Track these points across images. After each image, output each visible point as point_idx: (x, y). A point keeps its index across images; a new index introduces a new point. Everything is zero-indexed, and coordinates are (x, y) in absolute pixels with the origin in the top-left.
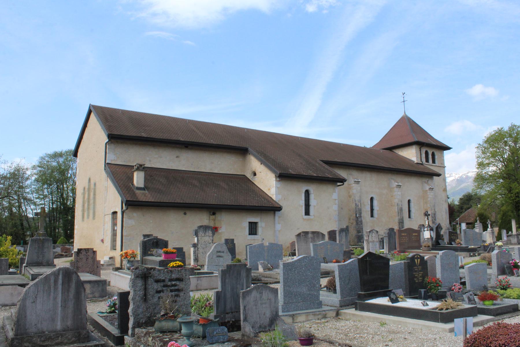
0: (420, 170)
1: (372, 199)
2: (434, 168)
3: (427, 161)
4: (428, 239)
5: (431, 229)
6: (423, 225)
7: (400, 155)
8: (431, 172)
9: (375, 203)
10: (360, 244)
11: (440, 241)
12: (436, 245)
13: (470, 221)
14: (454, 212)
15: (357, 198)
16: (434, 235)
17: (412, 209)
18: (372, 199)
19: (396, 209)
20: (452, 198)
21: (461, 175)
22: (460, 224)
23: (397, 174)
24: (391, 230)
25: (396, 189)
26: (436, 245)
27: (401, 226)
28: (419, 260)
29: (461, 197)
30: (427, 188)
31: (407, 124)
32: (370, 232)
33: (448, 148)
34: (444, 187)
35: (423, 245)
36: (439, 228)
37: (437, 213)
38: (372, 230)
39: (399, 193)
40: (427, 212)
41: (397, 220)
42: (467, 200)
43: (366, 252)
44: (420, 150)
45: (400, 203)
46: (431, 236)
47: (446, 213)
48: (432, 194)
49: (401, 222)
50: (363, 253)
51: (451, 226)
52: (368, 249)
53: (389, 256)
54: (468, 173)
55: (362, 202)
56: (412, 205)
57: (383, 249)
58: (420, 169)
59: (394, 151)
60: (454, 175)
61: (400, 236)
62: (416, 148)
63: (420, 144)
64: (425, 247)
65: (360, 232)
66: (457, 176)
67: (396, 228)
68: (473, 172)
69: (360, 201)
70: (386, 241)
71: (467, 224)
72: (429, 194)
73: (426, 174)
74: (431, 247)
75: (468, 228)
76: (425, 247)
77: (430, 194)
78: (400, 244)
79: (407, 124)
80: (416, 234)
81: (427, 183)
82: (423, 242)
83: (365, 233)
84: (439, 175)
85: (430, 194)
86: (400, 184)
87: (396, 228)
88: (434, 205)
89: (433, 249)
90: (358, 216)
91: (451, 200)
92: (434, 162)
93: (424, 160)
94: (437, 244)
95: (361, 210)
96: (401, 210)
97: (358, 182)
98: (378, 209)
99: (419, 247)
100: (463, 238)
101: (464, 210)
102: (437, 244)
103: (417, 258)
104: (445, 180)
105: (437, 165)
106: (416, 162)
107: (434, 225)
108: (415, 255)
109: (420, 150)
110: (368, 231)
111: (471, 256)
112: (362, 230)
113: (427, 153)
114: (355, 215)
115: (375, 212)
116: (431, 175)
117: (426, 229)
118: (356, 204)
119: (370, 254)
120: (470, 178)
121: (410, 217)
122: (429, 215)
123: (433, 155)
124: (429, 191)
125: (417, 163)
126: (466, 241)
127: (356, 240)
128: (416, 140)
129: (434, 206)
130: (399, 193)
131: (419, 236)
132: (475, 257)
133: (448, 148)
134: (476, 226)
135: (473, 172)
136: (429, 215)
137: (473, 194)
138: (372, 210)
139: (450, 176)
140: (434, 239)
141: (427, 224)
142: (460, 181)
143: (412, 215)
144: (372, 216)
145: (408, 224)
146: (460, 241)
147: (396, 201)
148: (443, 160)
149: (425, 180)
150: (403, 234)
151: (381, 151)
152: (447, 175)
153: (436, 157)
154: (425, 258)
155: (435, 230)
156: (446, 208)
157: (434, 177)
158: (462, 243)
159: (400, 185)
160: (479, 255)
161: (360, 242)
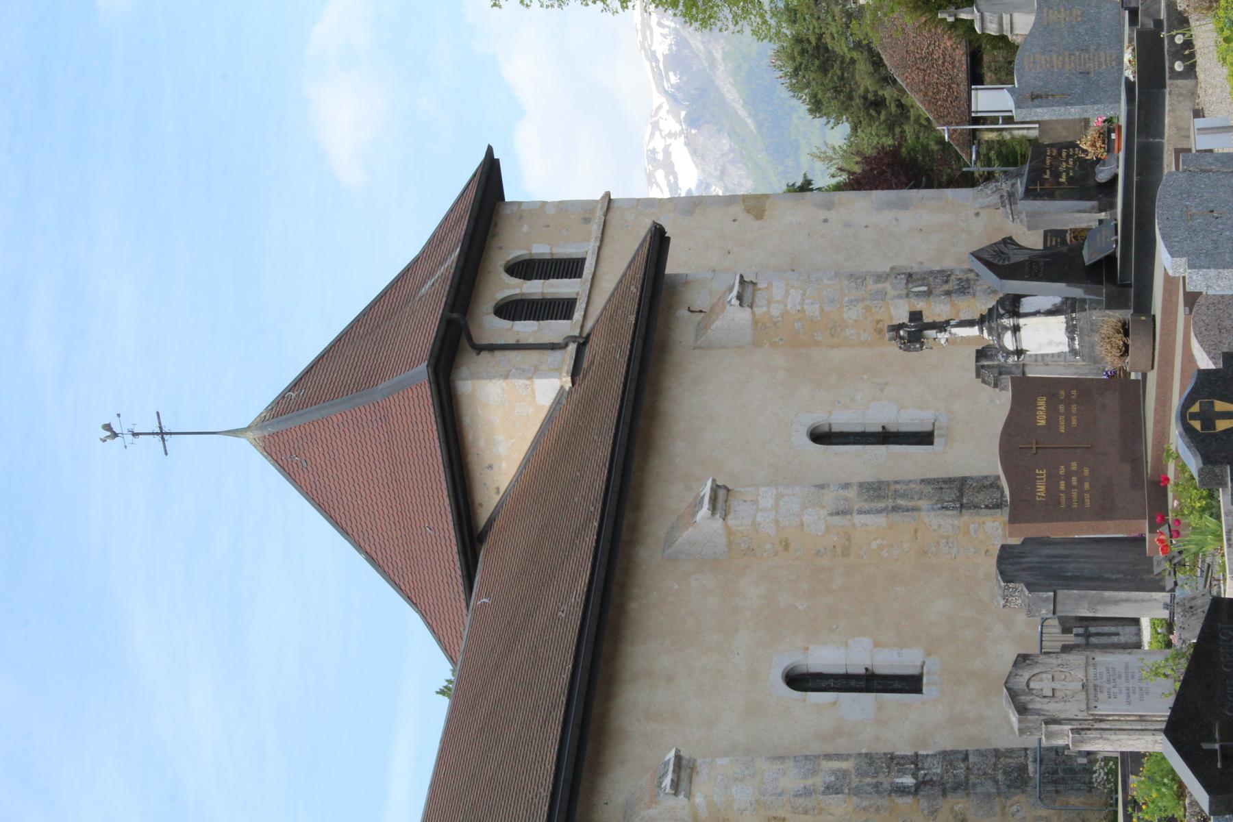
0: (621, 357)
1: (798, 680)
2: (615, 267)
3: (562, 308)
4: (1071, 330)
5: (1012, 306)
6: (981, 354)
7: (516, 480)
8: (635, 290)
9: (826, 657)
10: (1099, 775)
11: (1089, 256)
12: (1111, 277)
13: (961, 56)
14: (898, 166)
15: (792, 780)
16: (1043, 295)
17: (875, 417)
18: (798, 680)
19: (871, 525)
20: (805, 160)
21: (659, 99)
22: (976, 121)
23: (638, 507)
24: (1010, 563)
25: (741, 517)
26: (1111, 277)
27: (981, 498)
28: (1220, 406)
29: (800, 108)
30: (743, 316)
31: (309, 427)
32: (1022, 710)
33: (489, 175)
34: (737, 210)
35: (1111, 361)
36: (1002, 260)
37: (906, 261)
38: (1013, 695)
39: (766, 498)
40: (896, 328)
41: (940, 523)
42: (824, 69)
43: (1157, 744)
44: (492, 348)
45: (829, 497)
46: (1050, 313)
47: (904, 206)
48: (778, 292)
49: (959, 493)
50: (1161, 758)
51: (989, 177)
52: (1141, 724)
53: (1190, 588)
54: (652, 56)
55: (816, 748)
56: (843, 420)
57: (1136, 622)
58: (611, 356)
59: (484, 515)
60: (658, 143)
61: (1052, 509)
62: (475, 376)
63: (452, 347)
64: (1125, 351)
65: (1023, 769)
66: (670, 124)
67: (994, 530)
68: (646, 25)
69: (811, 761)
70: (1080, 604)
71: (976, 78)
72: (775, 311)
73: (648, 329)
74: (1127, 314)
75: (1005, 76)
76: (1125, 351)
77: (781, 298)
78: (1105, 510)
79: (309, 427)
80: (1042, 403)
81: (706, 316)
82: (1095, 360)
83: (1030, 741)
84: (659, 241)
85: (781, 298)
86: (707, 491)
87: (994, 530)
88: (852, 277)
89: (1143, 305)
90: (908, 780)
91: (819, 165)
92: (570, 268)
93: (556, 329)
94: (1110, 277)
95: (870, 758)
96: (875, 490)
97: (683, 769)
98: (866, 642)
99: (1128, 392)
100: (1074, 112)
101: (888, 93)
102: (1110, 277)
103: (1208, 418)
104: (693, 205)
105: (592, 245)
106: (567, 383)
107: (979, 288)
108: (1188, 430)
109: (492, 348)
110: (1014, 718)
111: (1190, 71)
112: (1009, 752)
113: (512, 309)
114: (905, 802)
115: (888, 661)
116: (655, 287)
117: (1008, 341)
118: (830, 789)
119: (1180, 729)
120: (681, 43)
121: (925, 438)
122: (916, 316)
123: (525, 269)
124: (731, 521)
125: (575, 374)
126: (1089, 87)
127: (1075, 800)
128: (422, 370)
129: (857, 278)
130: (766, 498)
131: (1050, 387)
132: (1198, 44)
133: (489, 175)
134: (992, 30)
135: (646, 25)
136: (916, 316)
137: (787, 31)
138: (870, 682)
139: (668, 166)
140: (1077, 292)
141: (974, 331)
142: (699, 107)
143: (910, 419)
144: (910, 684)
145: (974, 448)
146: (1092, 133)
147: (816, 520)
148: (562, 206)
149: (684, 330)
150: (1041, 489)
151: (480, 599)
152: (660, 192)
153: (541, 250)
154: (1205, 362)
155: (1014, 286)
156: (871, 209)
157: (671, 268)
158: (1097, 121)
159: (715, 489)
160: (1181, 21)
161: (1088, 770)
